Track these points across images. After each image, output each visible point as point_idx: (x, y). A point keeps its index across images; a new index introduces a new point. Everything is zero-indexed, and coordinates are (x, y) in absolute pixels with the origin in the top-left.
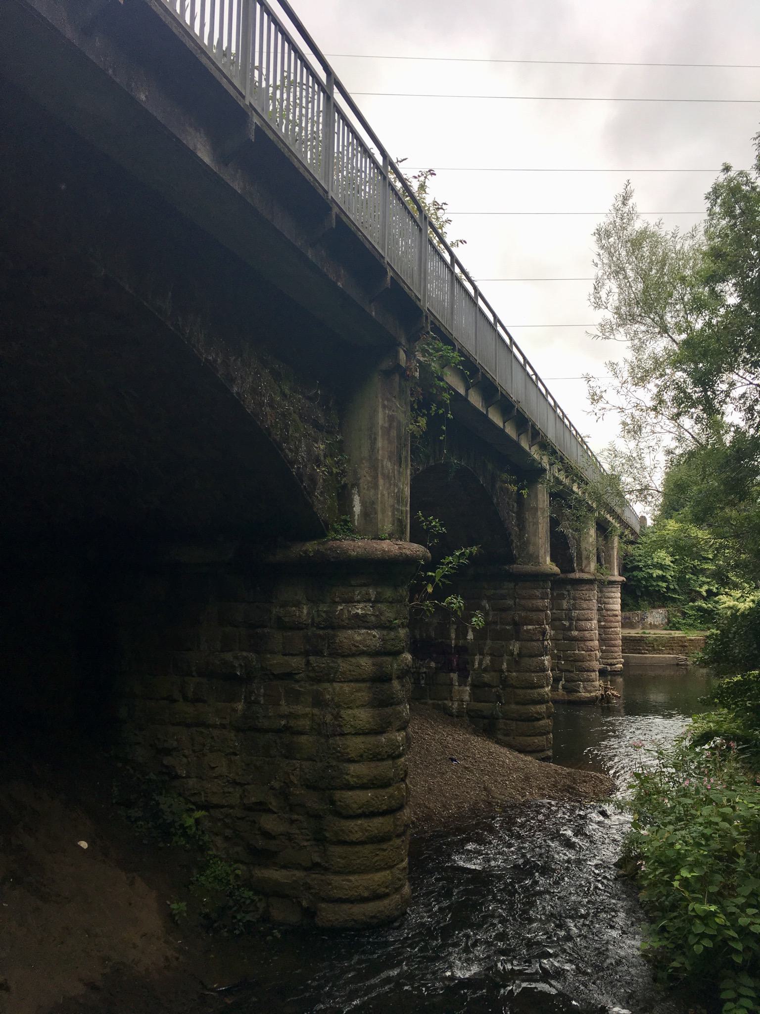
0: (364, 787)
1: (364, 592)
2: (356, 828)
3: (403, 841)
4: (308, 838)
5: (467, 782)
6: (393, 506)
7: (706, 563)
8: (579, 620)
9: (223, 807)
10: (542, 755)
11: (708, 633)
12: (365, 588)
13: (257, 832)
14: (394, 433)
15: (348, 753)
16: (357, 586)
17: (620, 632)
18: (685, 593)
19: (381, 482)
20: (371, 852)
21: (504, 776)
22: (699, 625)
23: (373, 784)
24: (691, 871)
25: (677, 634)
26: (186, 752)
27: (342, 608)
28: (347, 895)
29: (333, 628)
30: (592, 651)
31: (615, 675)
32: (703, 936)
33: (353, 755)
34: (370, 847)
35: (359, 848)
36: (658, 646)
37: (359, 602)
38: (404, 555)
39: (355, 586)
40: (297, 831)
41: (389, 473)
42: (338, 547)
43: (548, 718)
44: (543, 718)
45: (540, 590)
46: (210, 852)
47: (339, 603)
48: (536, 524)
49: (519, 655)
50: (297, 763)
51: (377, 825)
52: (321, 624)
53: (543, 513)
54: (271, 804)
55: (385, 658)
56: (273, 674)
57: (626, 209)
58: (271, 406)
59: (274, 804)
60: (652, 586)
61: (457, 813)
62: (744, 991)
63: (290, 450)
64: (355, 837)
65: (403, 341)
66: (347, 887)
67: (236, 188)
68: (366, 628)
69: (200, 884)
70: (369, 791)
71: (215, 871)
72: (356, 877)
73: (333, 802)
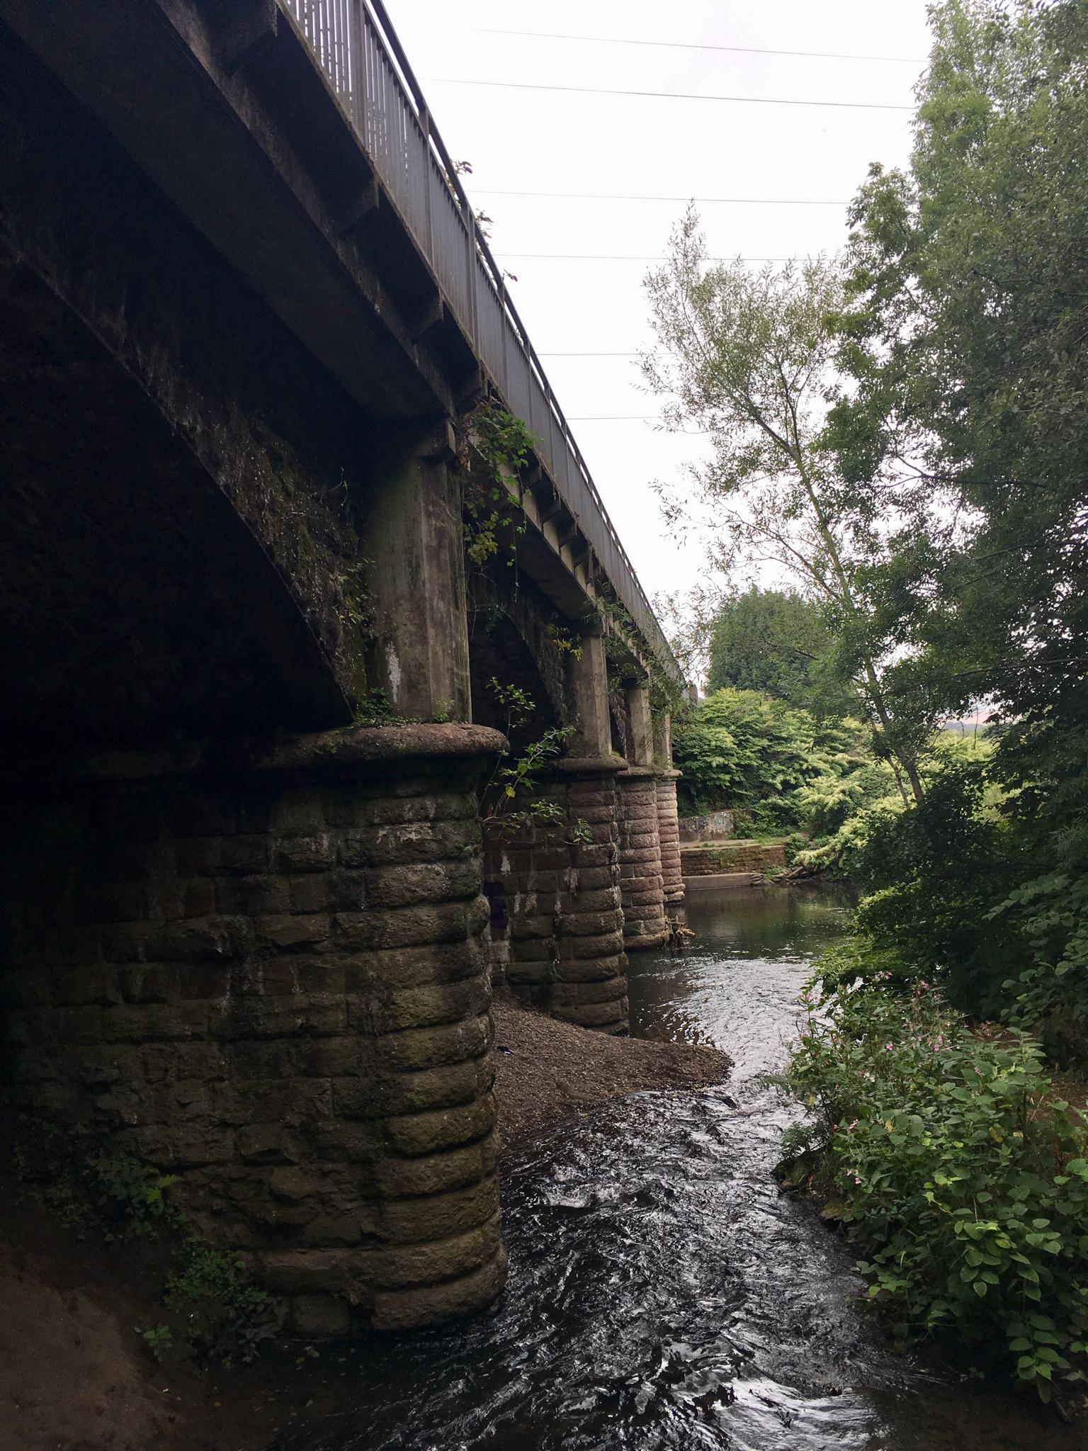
0: (435, 1107)
1: (418, 806)
2: (426, 1172)
3: (495, 1182)
4: (353, 1196)
5: (530, 1079)
6: (452, 669)
7: (779, 744)
8: (635, 833)
9: (205, 1164)
10: (617, 1028)
11: (788, 839)
12: (419, 800)
13: (267, 1198)
14: (445, 556)
15: (408, 1058)
16: (406, 797)
17: (679, 846)
18: (755, 787)
19: (431, 632)
20: (454, 1206)
21: (577, 1064)
22: (775, 829)
23: (448, 1100)
24: (949, 1174)
25: (748, 843)
26: (135, 1084)
27: (385, 833)
28: (419, 1276)
29: (372, 865)
30: (653, 875)
31: (674, 907)
32: (983, 1268)
33: (417, 1059)
34: (450, 1198)
35: (433, 1203)
36: (725, 862)
37: (410, 822)
38: (477, 744)
39: (402, 797)
40: (335, 1189)
41: (442, 618)
42: (377, 737)
43: (622, 974)
44: (616, 975)
45: (603, 793)
46: (191, 1239)
47: (381, 825)
48: (592, 697)
49: (578, 888)
50: (326, 1082)
51: (459, 1162)
52: (353, 861)
53: (599, 681)
54: (286, 1149)
55: (455, 906)
56: (277, 946)
57: (689, 242)
58: (273, 512)
59: (293, 1150)
60: (712, 779)
61: (526, 1127)
62: (1041, 1337)
63: (300, 581)
64: (427, 1186)
65: (451, 410)
66: (419, 1265)
67: (244, 119)
68: (423, 861)
69: (180, 1292)
70: (443, 1112)
71: (202, 1269)
72: (433, 1247)
73: (389, 1136)
